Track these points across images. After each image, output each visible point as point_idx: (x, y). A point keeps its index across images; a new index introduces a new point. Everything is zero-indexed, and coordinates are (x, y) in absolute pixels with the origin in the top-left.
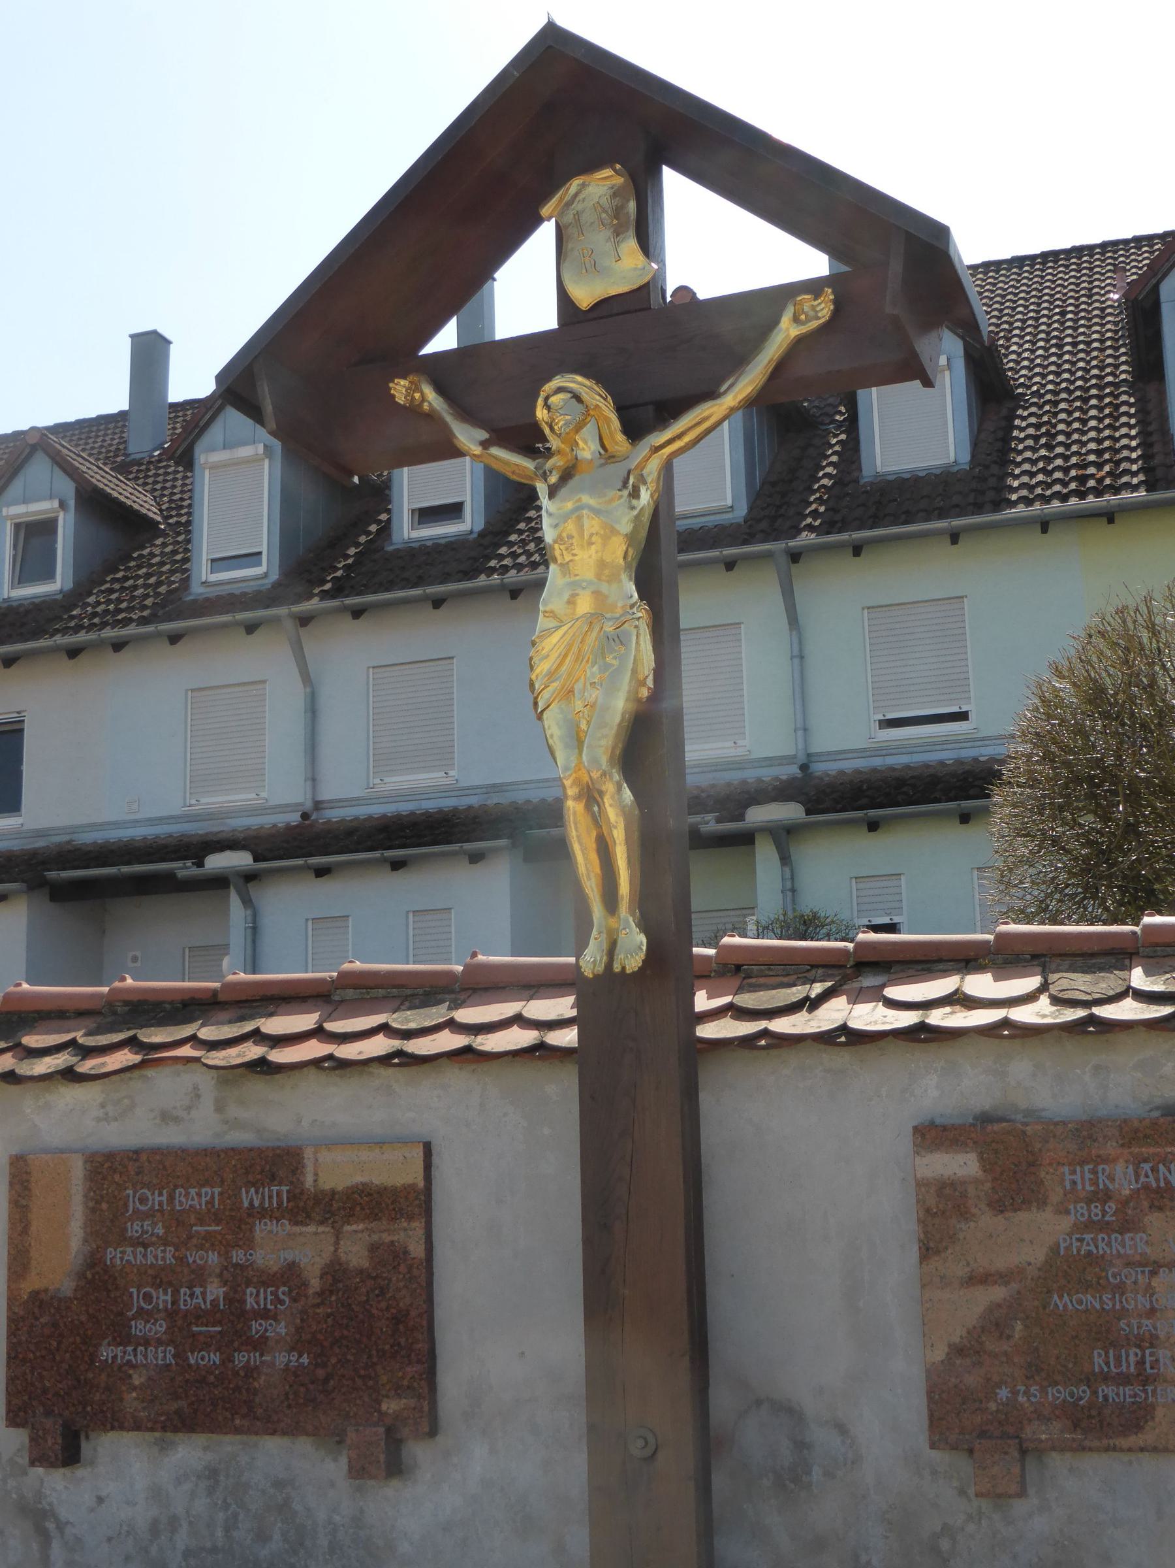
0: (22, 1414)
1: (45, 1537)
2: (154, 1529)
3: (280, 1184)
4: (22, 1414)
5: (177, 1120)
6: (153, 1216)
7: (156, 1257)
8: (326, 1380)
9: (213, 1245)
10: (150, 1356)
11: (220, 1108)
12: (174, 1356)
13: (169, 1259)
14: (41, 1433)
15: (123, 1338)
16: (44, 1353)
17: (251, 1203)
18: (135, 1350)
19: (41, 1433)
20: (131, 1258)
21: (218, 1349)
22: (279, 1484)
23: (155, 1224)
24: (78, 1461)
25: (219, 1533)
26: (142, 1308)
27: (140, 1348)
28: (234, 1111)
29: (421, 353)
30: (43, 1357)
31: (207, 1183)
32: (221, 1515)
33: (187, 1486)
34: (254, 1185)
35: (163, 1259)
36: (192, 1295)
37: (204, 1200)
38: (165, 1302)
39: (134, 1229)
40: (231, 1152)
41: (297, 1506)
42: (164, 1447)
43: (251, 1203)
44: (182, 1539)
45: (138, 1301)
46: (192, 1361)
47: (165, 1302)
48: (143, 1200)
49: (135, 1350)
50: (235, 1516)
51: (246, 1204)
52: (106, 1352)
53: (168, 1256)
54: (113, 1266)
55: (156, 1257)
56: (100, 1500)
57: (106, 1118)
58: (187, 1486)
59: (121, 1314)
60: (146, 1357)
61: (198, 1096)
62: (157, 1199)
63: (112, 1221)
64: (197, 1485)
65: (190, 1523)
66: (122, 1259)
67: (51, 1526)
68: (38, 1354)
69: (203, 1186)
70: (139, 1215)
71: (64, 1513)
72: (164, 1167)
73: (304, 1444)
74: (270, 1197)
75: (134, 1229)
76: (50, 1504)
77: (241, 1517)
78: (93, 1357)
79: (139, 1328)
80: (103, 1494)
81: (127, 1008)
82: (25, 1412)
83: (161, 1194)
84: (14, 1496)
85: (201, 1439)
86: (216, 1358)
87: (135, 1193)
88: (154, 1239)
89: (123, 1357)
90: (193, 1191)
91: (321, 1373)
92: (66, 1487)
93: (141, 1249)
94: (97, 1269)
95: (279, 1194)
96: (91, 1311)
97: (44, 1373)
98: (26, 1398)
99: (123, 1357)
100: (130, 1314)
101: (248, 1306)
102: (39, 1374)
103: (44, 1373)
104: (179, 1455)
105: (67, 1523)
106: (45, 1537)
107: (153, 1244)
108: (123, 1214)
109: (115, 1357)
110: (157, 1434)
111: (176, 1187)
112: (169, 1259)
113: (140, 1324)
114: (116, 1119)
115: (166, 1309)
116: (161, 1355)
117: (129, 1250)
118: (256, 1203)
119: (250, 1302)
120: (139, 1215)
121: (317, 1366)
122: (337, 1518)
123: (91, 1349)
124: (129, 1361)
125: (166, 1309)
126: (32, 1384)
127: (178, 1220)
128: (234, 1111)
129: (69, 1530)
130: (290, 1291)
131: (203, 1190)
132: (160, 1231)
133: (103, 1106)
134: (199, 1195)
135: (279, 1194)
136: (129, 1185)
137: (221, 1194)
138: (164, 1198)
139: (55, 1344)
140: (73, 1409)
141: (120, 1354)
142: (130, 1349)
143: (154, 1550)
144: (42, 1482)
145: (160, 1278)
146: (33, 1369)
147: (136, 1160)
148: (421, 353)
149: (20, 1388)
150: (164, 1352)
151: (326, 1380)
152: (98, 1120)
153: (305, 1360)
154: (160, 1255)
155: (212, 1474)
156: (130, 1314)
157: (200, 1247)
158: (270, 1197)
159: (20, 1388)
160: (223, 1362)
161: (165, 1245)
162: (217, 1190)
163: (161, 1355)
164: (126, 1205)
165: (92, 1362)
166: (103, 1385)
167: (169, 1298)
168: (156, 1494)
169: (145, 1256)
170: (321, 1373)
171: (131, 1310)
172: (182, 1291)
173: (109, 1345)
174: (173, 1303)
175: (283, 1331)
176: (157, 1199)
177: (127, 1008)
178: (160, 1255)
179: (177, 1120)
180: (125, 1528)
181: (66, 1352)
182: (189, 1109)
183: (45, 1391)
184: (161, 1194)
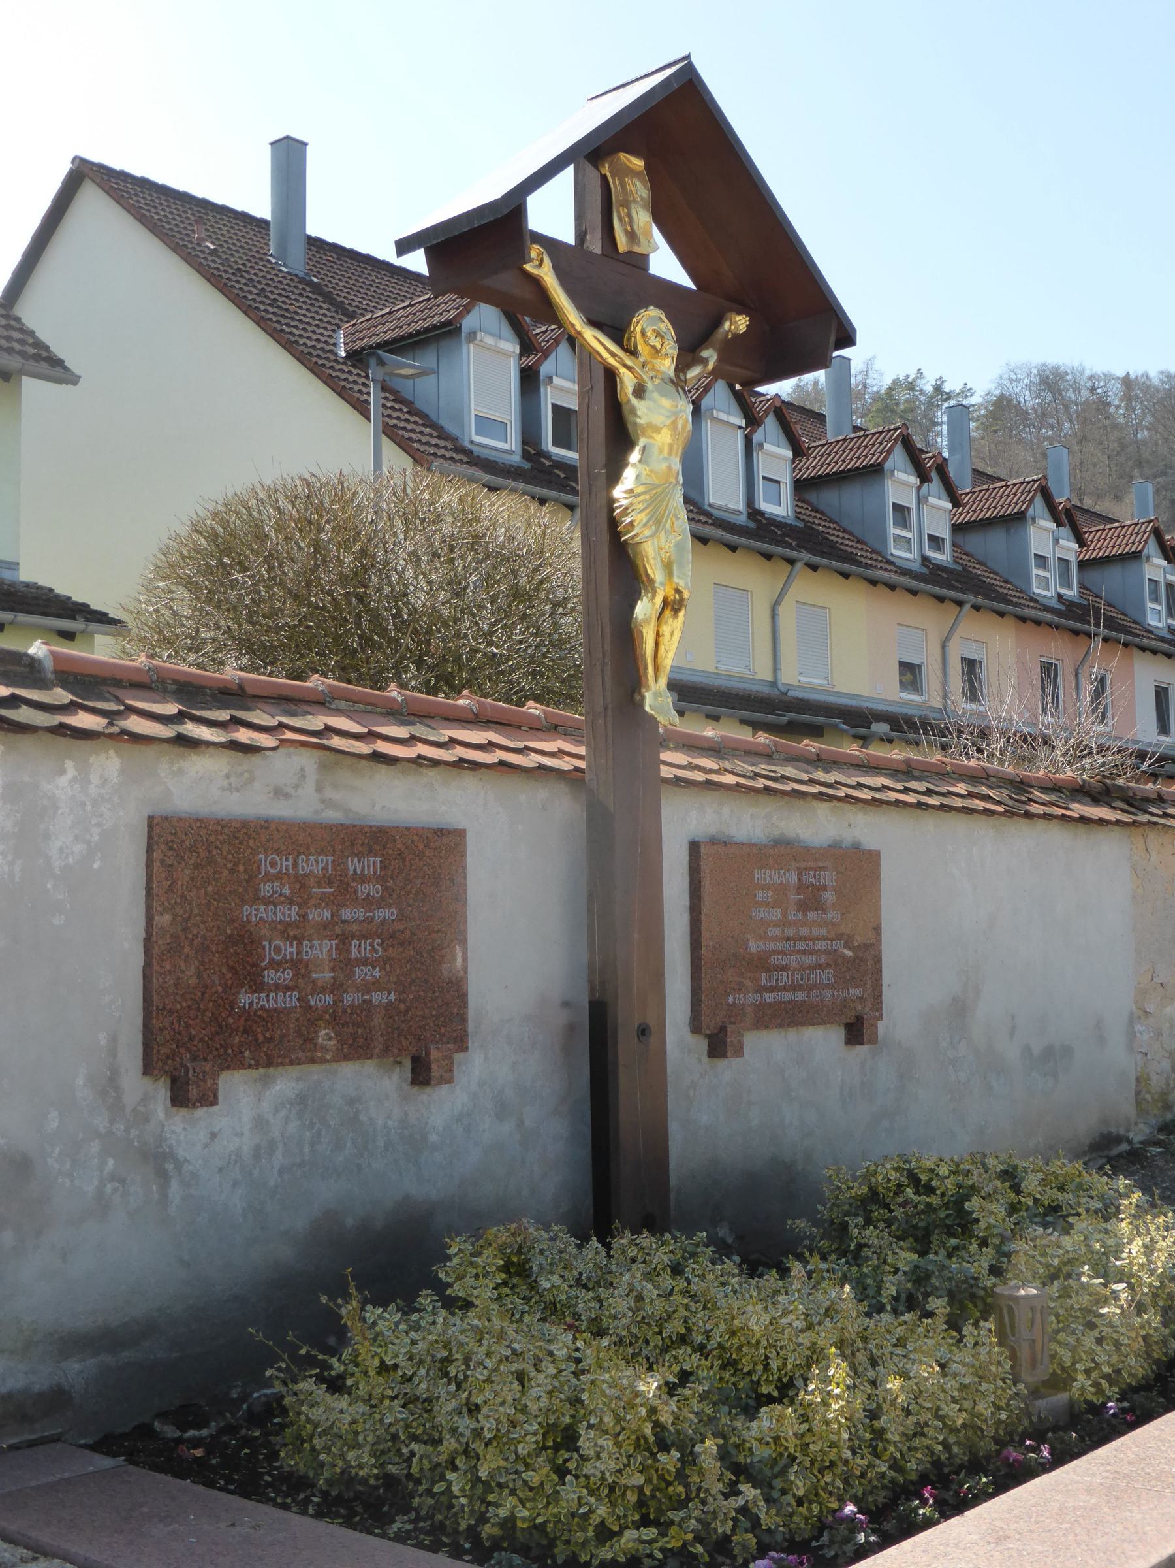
0: (170, 1062)
1: (163, 1176)
2: (257, 1153)
3: (375, 856)
4: (170, 1062)
5: (287, 796)
6: (281, 879)
7: (284, 914)
8: (406, 1012)
9: (327, 904)
10: (280, 1001)
11: (319, 789)
12: (299, 1000)
13: (295, 917)
14: (201, 1076)
15: (258, 986)
16: (190, 1003)
17: (355, 870)
18: (267, 996)
19: (201, 1076)
20: (264, 915)
21: (332, 992)
22: (351, 1102)
23: (282, 885)
24: (173, 1105)
25: (307, 1149)
26: (273, 959)
27: (272, 994)
28: (329, 793)
29: (693, 287)
30: (189, 1007)
31: (321, 852)
32: (308, 1134)
33: (283, 1113)
34: (357, 855)
35: (290, 916)
36: (312, 947)
37: (320, 866)
38: (291, 953)
39: (266, 889)
40: (323, 826)
41: (363, 1118)
42: (266, 1082)
43: (355, 870)
44: (279, 1158)
45: (269, 954)
46: (313, 1003)
47: (291, 953)
48: (273, 864)
49: (267, 996)
50: (319, 1134)
51: (351, 871)
52: (244, 999)
53: (294, 913)
54: (249, 921)
55: (284, 914)
56: (213, 1136)
57: (230, 788)
58: (283, 1113)
59: (255, 965)
60: (276, 1001)
61: (304, 777)
62: (285, 864)
63: (248, 882)
64: (290, 1110)
65: (285, 1144)
66: (256, 916)
67: (170, 1166)
68: (184, 1004)
69: (320, 854)
70: (268, 878)
71: (181, 1153)
72: (290, 837)
73: (369, 1067)
74: (369, 866)
75: (266, 889)
76: (170, 1147)
77: (323, 1132)
78: (233, 1004)
79: (270, 976)
80: (216, 1130)
81: (175, 687)
82: (174, 1060)
83: (287, 860)
84: (136, 1144)
85: (294, 1071)
86: (330, 999)
87: (266, 857)
88: (282, 899)
89: (258, 1003)
90: (312, 858)
91: (402, 1006)
92: (185, 1129)
93: (271, 907)
94: (236, 925)
95: (374, 862)
96: (231, 963)
97: (191, 1022)
98: (174, 1046)
99: (258, 1003)
100: (263, 964)
101: (353, 956)
102: (186, 1023)
103: (191, 1022)
104: (278, 1088)
105: (186, 1160)
106: (163, 1176)
107: (282, 903)
108: (256, 876)
109: (251, 1004)
110: (262, 1071)
111: (299, 854)
112: (295, 917)
113: (272, 973)
114: (237, 790)
115: (292, 960)
116: (288, 999)
117: (262, 908)
118: (359, 871)
119: (354, 953)
120: (268, 878)
121: (400, 1001)
122: (390, 1123)
123: (231, 998)
124: (263, 1006)
125: (292, 960)
126: (179, 1033)
127: (301, 882)
128: (329, 793)
129: (187, 1168)
130: (382, 943)
131: (320, 858)
132: (287, 891)
133: (227, 776)
134: (317, 861)
135: (374, 862)
136: (261, 850)
137: (333, 861)
138: (290, 863)
139: (199, 994)
140: (216, 1053)
141: (256, 1000)
142: (263, 995)
143: (256, 1173)
144: (163, 1126)
145: (286, 930)
146: (180, 1019)
147: (267, 828)
148: (693, 287)
149: (168, 1038)
150: (291, 996)
151: (406, 1012)
152: (223, 789)
153: (392, 997)
154: (287, 912)
155: (301, 1100)
156: (263, 964)
157: (317, 906)
158: (369, 866)
159: (168, 1038)
160: (335, 1003)
161: (291, 904)
162: (330, 858)
163: (288, 999)
164: (259, 867)
165: (232, 1008)
166: (241, 1029)
167: (294, 950)
168: (260, 1123)
169: (275, 913)
170: (402, 1006)
171: (263, 960)
172: (305, 943)
173: (246, 992)
174: (297, 954)
175: (378, 975)
176: (285, 864)
177: (175, 687)
178: (287, 912)
179: (287, 796)
180: (233, 1157)
181: (210, 1000)
182: (297, 787)
183: (191, 1038)
184: (287, 860)
